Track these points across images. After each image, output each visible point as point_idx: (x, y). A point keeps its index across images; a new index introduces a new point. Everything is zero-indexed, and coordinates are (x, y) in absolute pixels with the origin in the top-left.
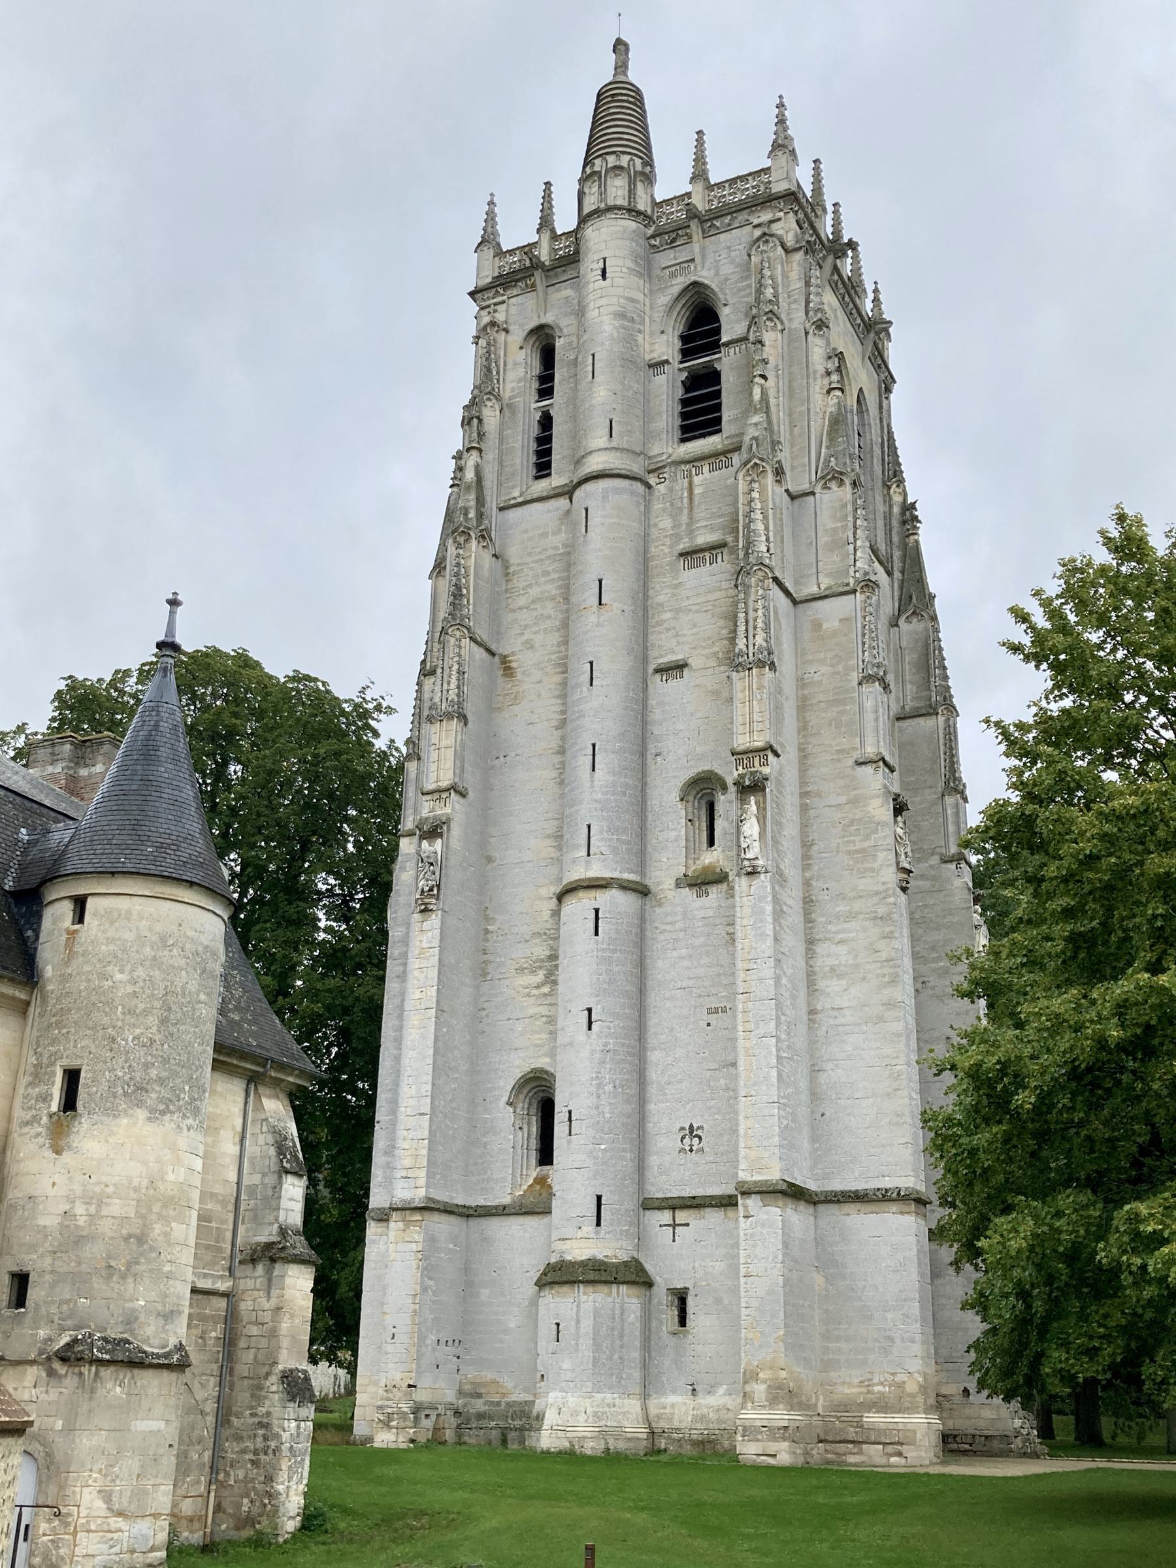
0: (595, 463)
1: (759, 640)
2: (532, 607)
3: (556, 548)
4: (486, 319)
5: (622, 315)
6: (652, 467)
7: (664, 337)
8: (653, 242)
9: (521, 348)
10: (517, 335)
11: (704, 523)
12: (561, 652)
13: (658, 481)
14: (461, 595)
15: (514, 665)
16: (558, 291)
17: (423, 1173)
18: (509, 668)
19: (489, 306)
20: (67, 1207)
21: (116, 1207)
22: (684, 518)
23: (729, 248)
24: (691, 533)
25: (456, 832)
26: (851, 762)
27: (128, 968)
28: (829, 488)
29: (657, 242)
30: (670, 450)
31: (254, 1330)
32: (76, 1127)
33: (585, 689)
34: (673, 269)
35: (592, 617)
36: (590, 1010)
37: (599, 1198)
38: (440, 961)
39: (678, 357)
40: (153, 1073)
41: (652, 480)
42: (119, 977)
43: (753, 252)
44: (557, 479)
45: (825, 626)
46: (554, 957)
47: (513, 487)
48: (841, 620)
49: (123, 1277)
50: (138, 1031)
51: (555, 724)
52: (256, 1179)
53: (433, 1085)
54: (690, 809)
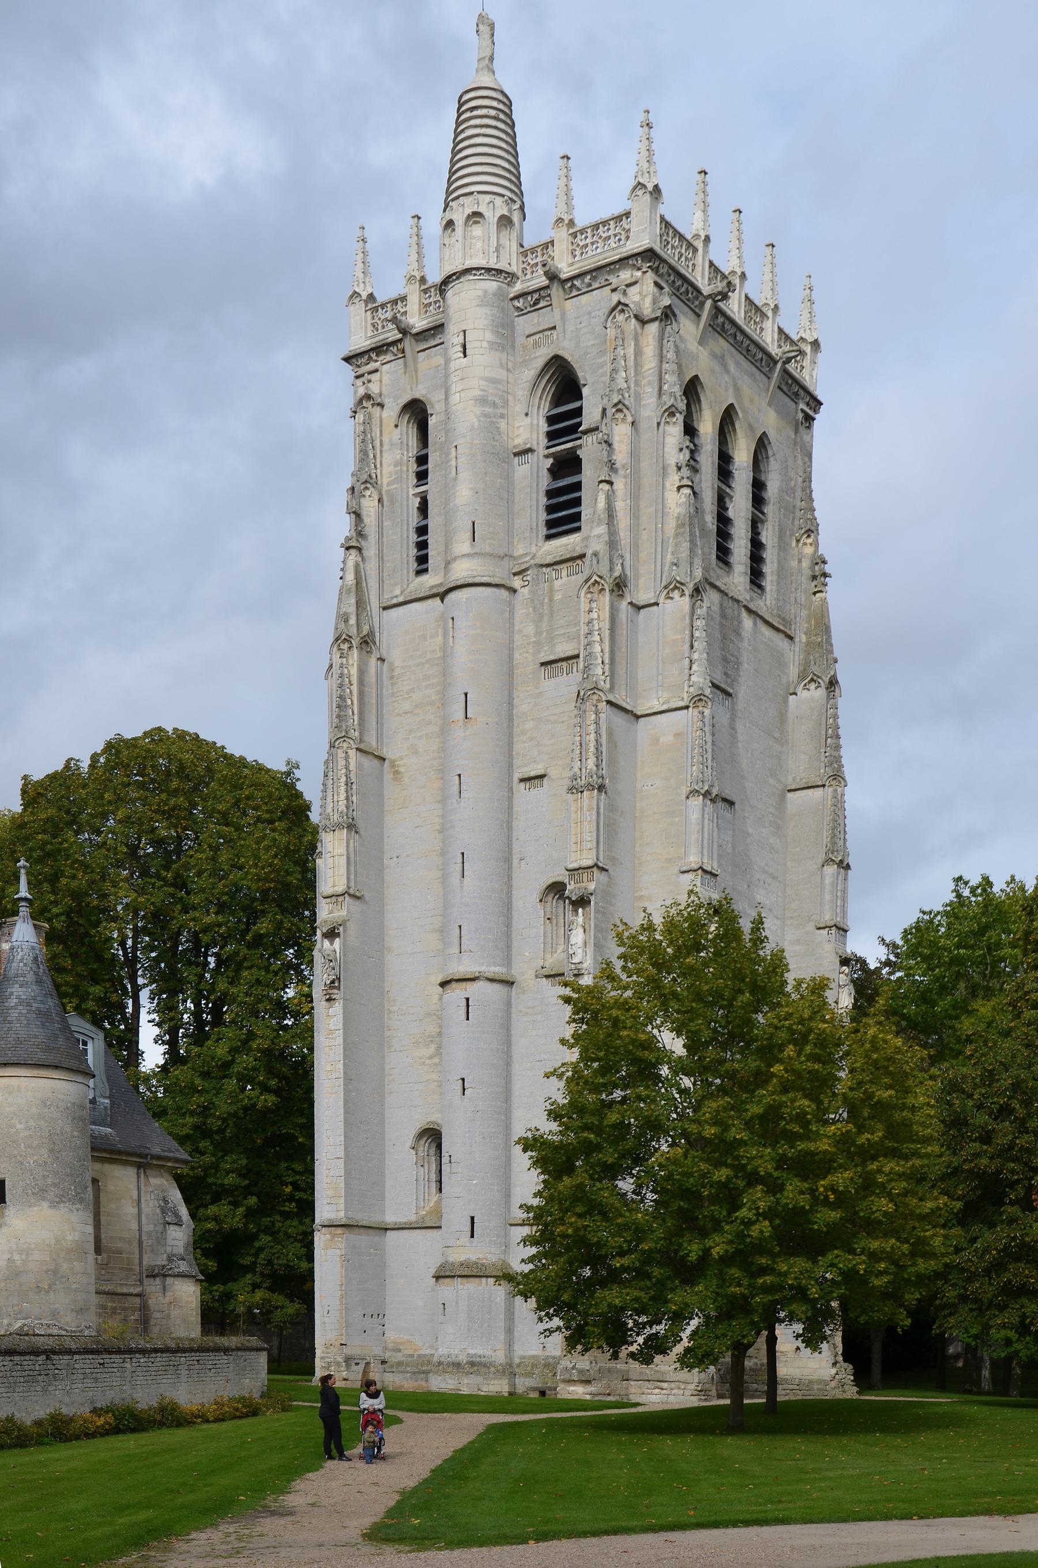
0: (462, 571)
1: (591, 764)
2: (415, 711)
3: (434, 651)
4: (361, 391)
5: (482, 401)
6: (516, 570)
7: (528, 420)
8: (516, 303)
9: (396, 426)
10: (391, 412)
11: (562, 632)
12: (440, 758)
13: (522, 583)
14: (346, 706)
15: (402, 769)
16: (428, 357)
17: (342, 1200)
18: (396, 772)
19: (362, 375)
20: (9, 1256)
21: (36, 1256)
22: (545, 625)
23: (589, 313)
24: (551, 640)
25: (352, 931)
26: (676, 871)
27: (23, 1121)
28: (672, 598)
29: (519, 303)
30: (534, 549)
31: (158, 1315)
32: (7, 1212)
33: (454, 801)
34: (537, 337)
35: (458, 733)
36: (463, 1080)
37: (472, 1218)
38: (345, 1040)
39: (544, 441)
40: (49, 1181)
41: (517, 582)
42: (19, 1126)
43: (609, 324)
44: (430, 581)
45: (661, 740)
46: (440, 1034)
47: (395, 585)
48: (675, 735)
49: (47, 1292)
50: (36, 1158)
51: (438, 827)
52: (151, 1227)
53: (345, 1136)
54: (549, 909)
